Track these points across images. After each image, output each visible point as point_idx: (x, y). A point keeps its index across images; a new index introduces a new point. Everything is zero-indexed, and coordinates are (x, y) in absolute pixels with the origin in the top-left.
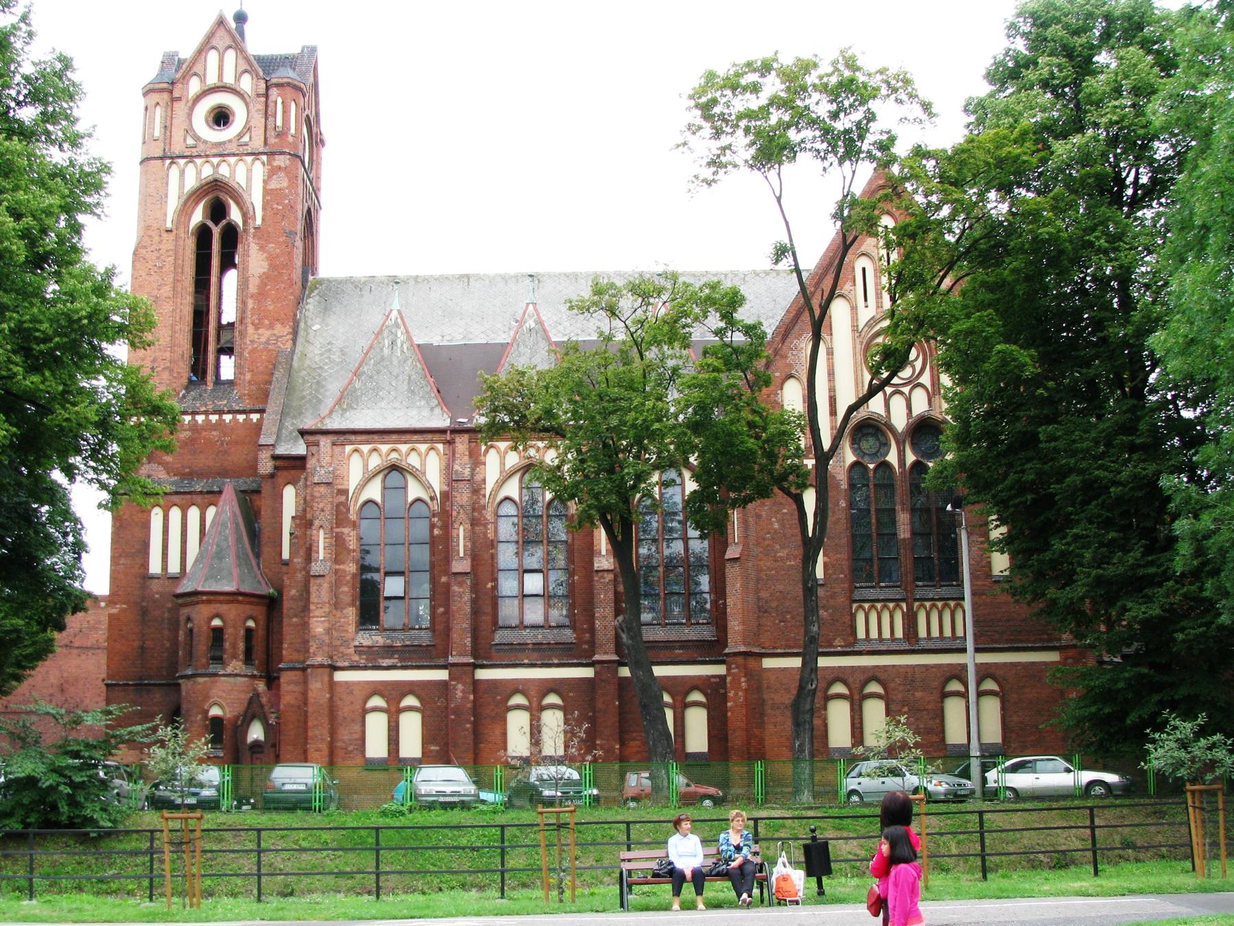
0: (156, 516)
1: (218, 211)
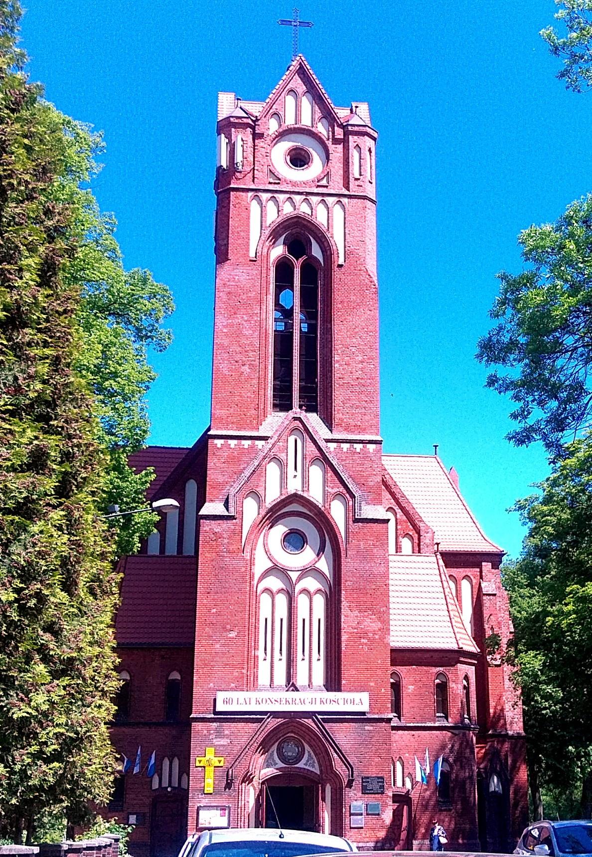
1: (297, 246)
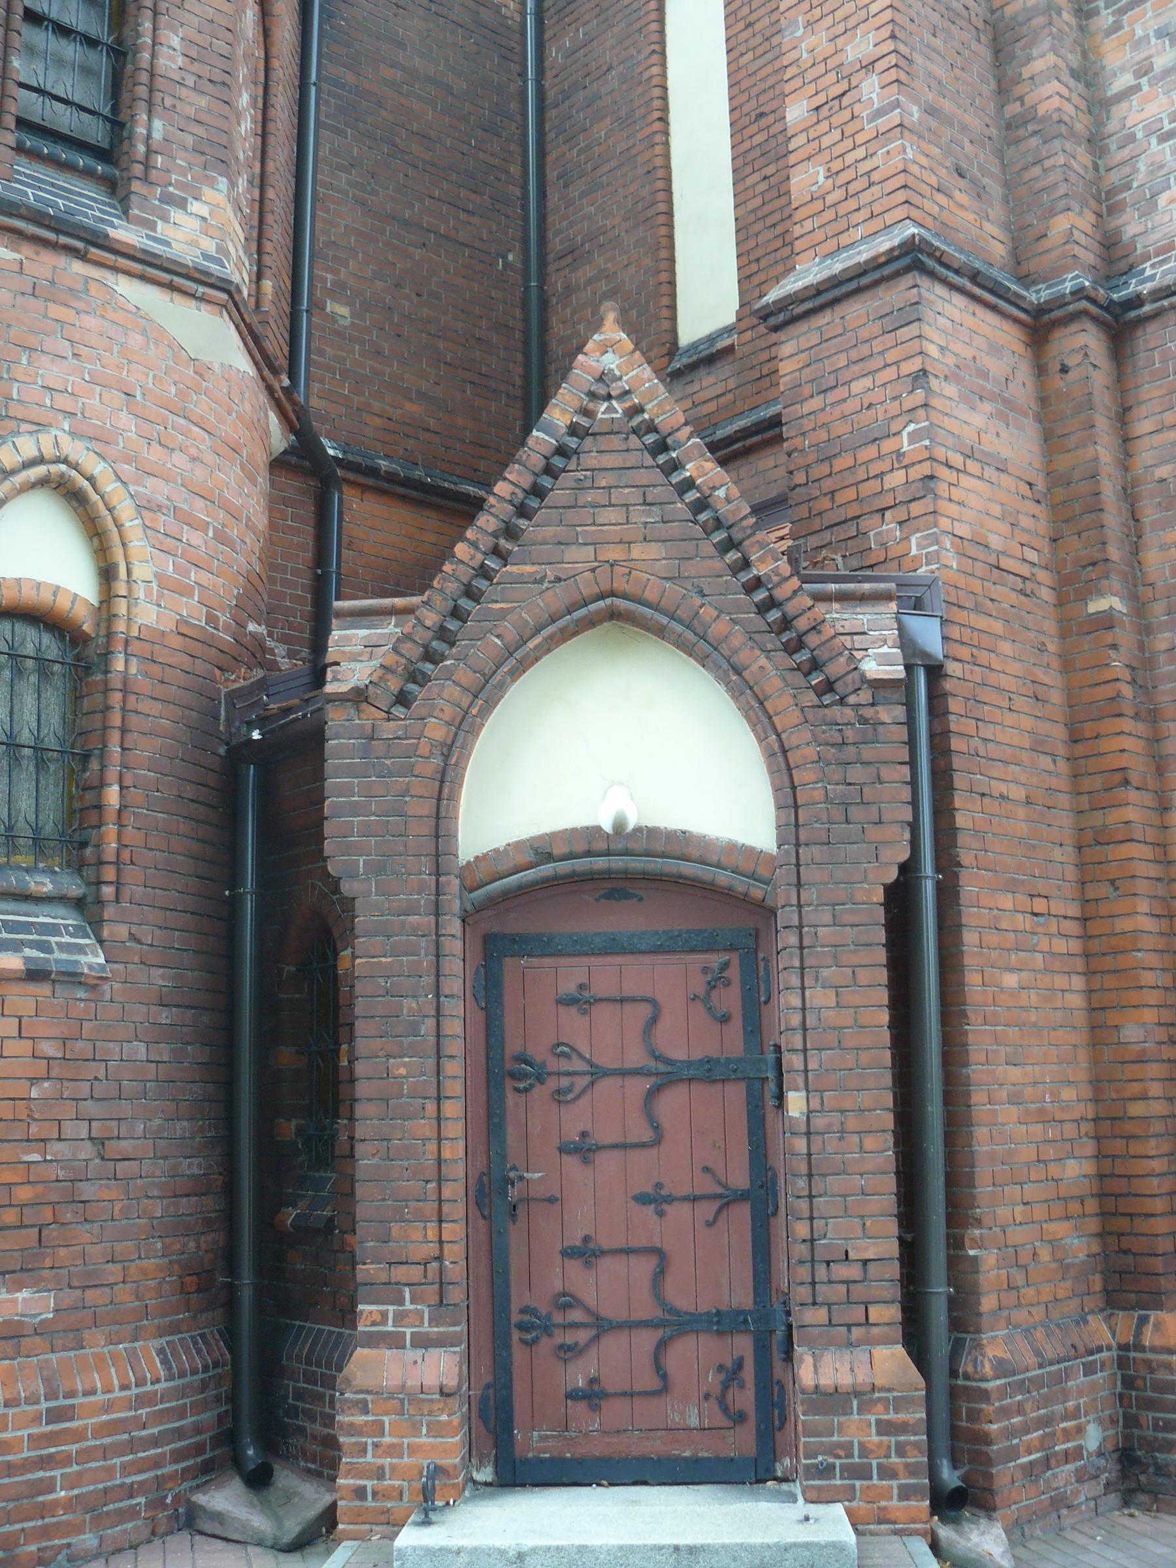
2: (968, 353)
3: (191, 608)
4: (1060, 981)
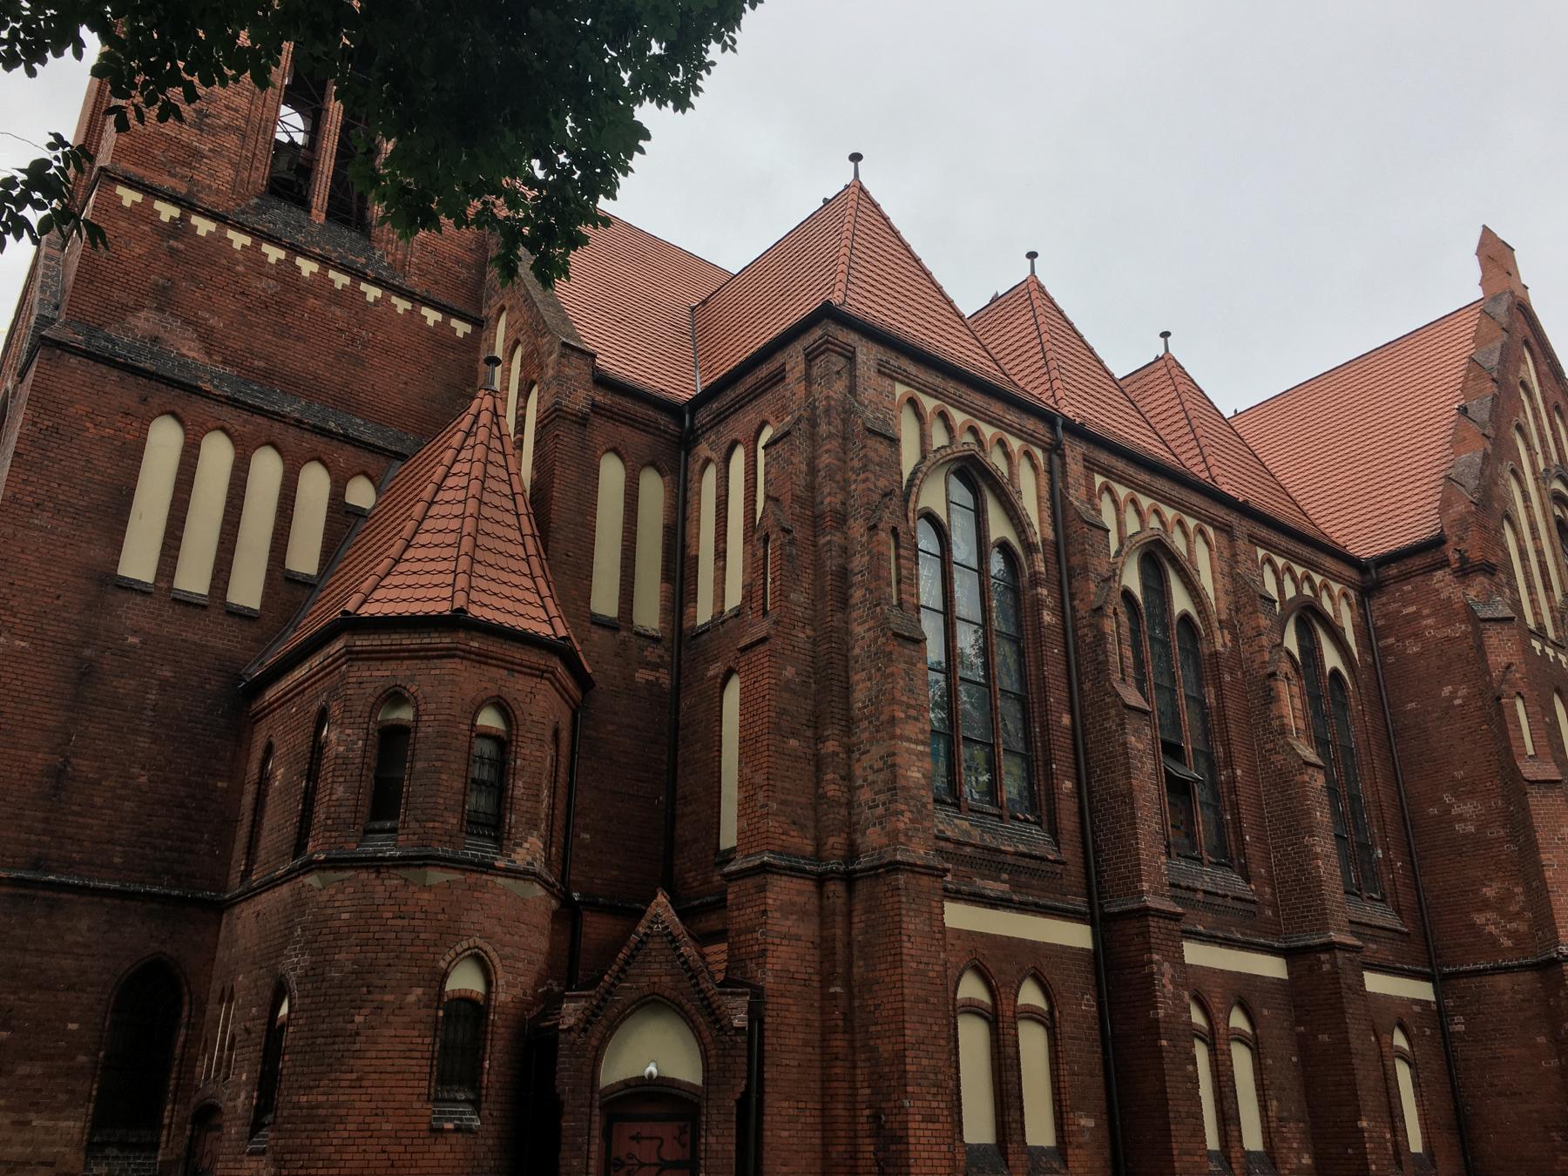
0: (165, 439)
2: (787, 898)
3: (517, 991)
4: (810, 1134)
